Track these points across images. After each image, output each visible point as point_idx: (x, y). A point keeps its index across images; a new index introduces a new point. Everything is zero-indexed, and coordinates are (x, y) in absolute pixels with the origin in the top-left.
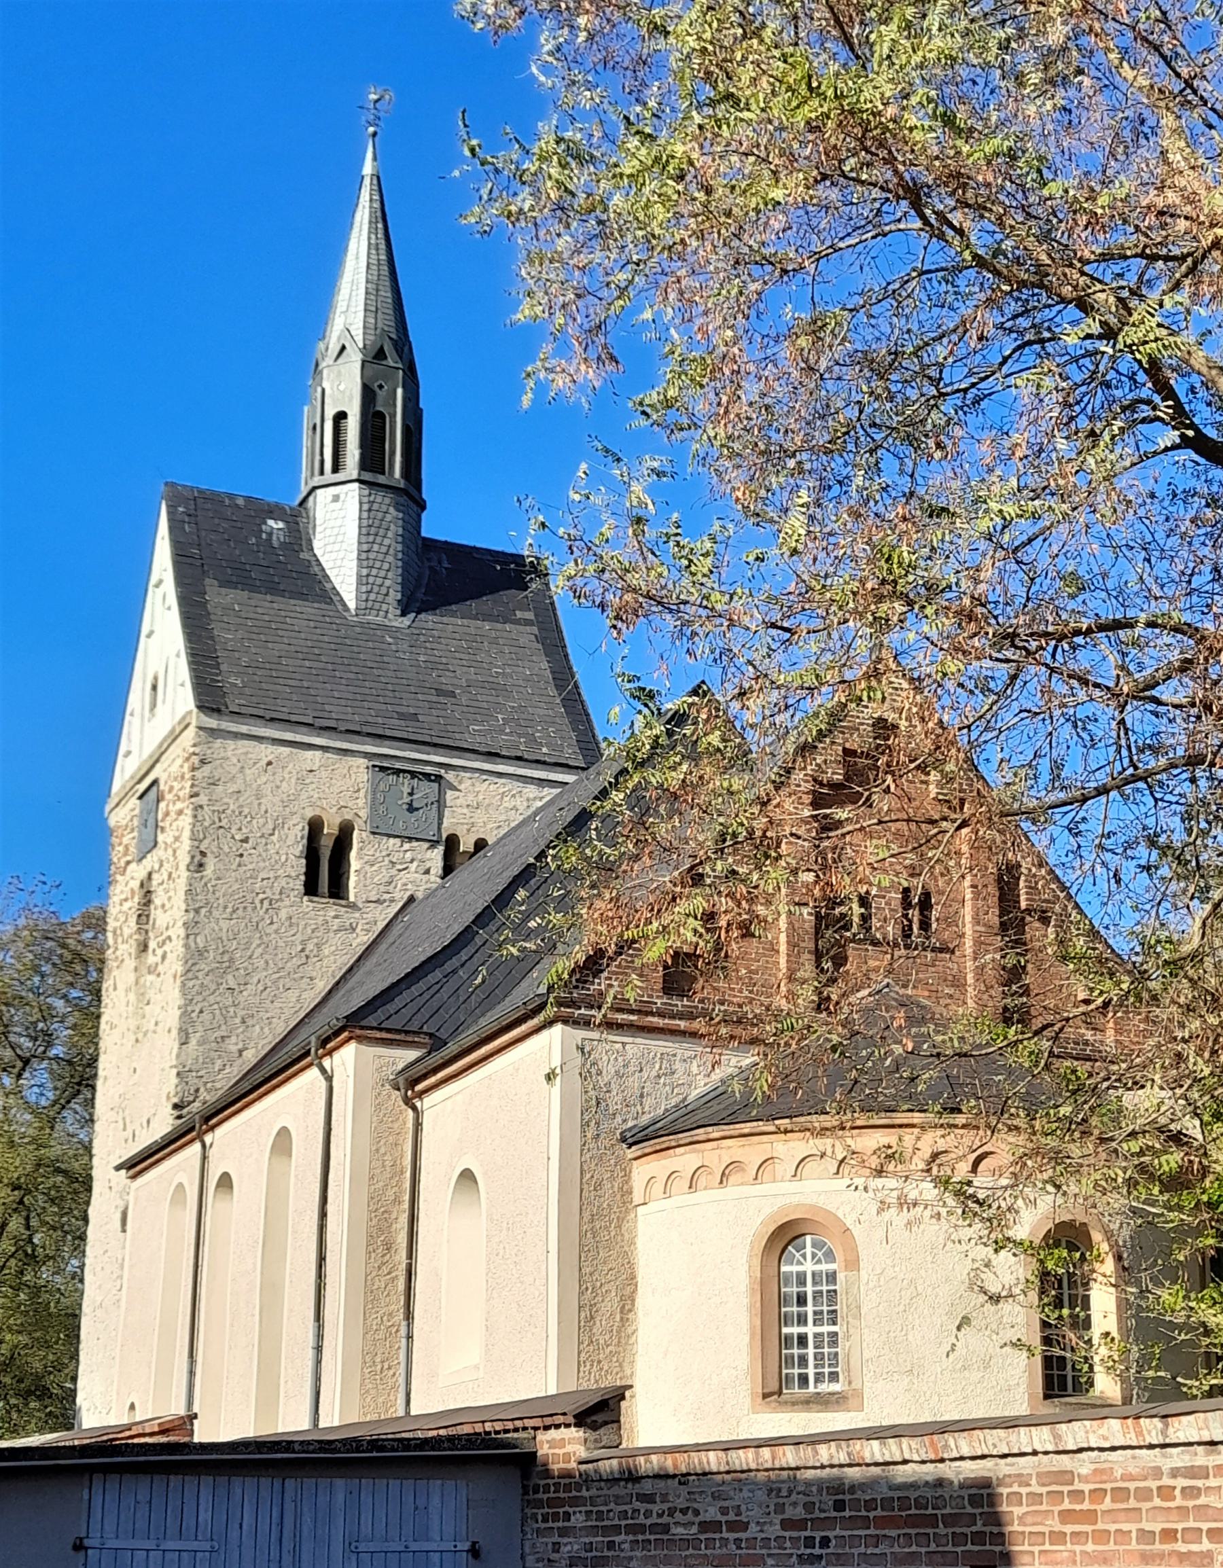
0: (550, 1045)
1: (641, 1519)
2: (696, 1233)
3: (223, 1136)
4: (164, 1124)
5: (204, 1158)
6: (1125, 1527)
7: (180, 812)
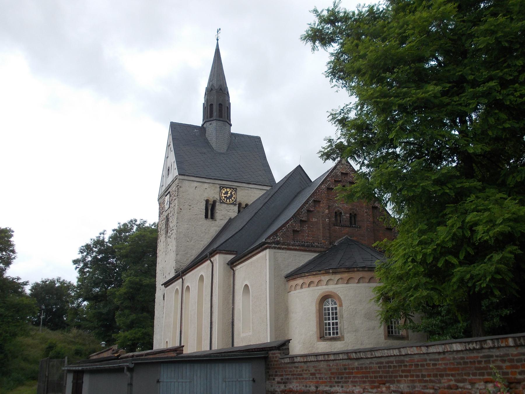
0: (266, 254)
1: (295, 373)
2: (304, 300)
3: (187, 277)
4: (172, 275)
5: (183, 282)
6: (418, 374)
7: (175, 199)
